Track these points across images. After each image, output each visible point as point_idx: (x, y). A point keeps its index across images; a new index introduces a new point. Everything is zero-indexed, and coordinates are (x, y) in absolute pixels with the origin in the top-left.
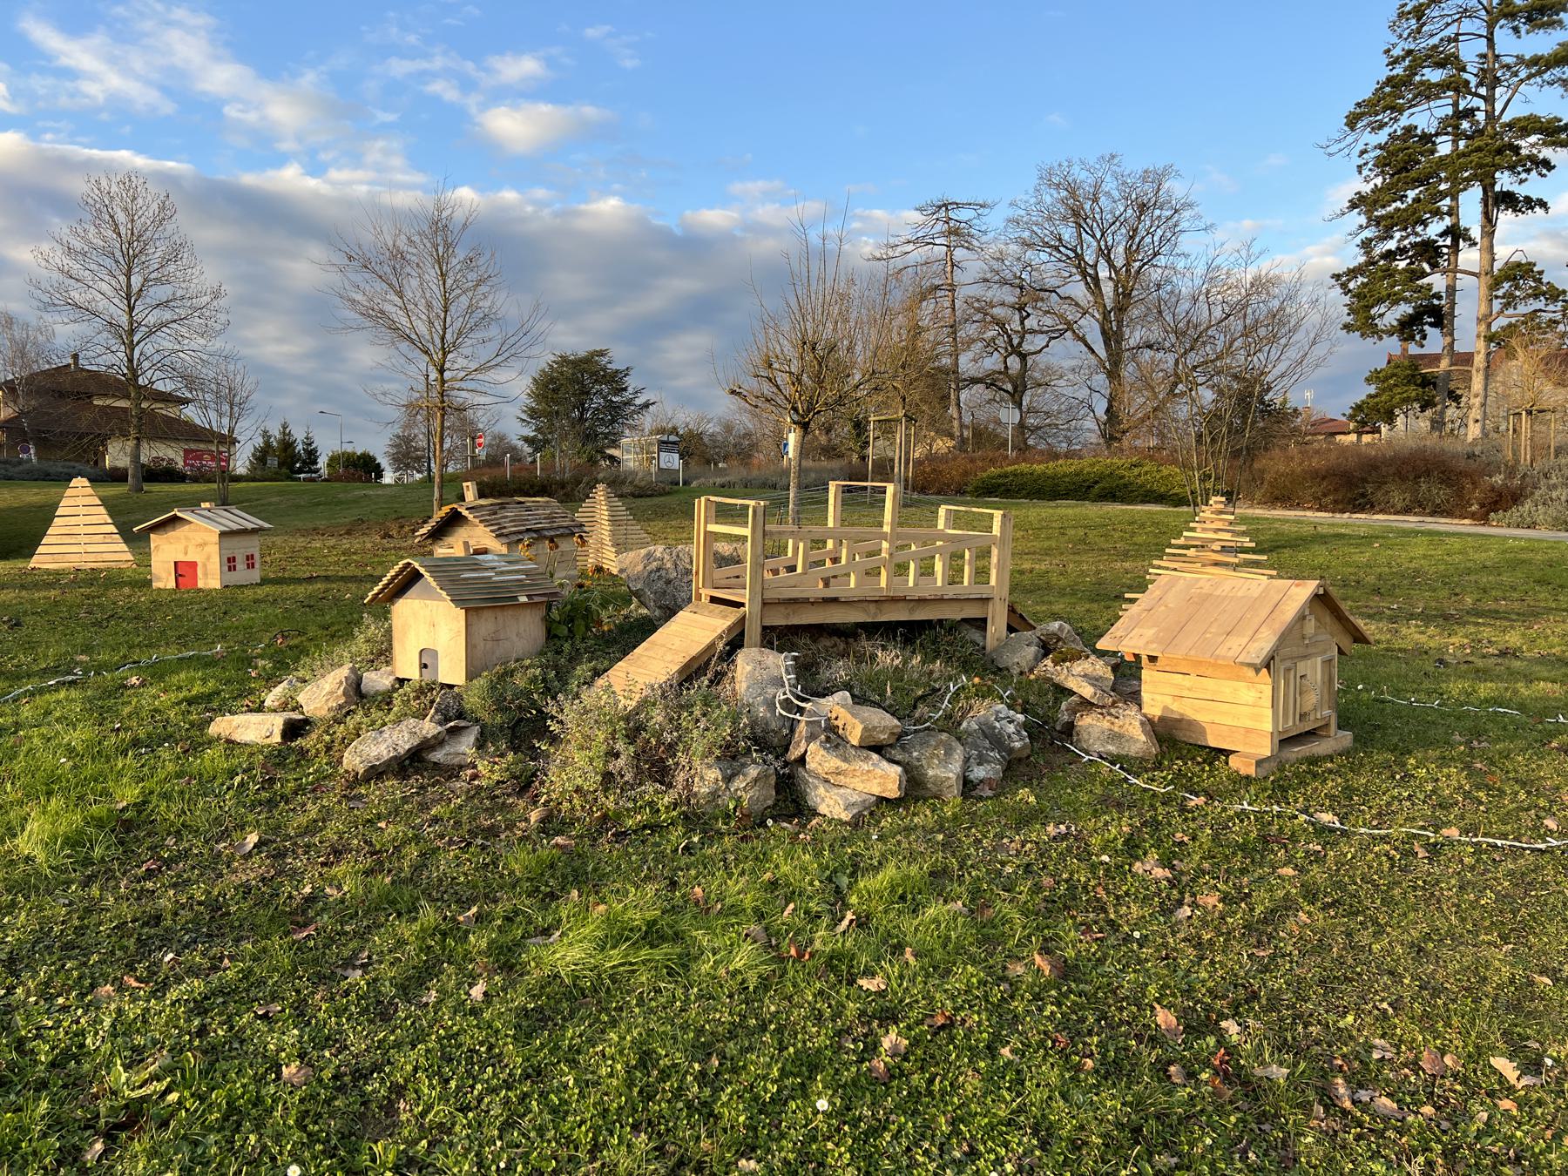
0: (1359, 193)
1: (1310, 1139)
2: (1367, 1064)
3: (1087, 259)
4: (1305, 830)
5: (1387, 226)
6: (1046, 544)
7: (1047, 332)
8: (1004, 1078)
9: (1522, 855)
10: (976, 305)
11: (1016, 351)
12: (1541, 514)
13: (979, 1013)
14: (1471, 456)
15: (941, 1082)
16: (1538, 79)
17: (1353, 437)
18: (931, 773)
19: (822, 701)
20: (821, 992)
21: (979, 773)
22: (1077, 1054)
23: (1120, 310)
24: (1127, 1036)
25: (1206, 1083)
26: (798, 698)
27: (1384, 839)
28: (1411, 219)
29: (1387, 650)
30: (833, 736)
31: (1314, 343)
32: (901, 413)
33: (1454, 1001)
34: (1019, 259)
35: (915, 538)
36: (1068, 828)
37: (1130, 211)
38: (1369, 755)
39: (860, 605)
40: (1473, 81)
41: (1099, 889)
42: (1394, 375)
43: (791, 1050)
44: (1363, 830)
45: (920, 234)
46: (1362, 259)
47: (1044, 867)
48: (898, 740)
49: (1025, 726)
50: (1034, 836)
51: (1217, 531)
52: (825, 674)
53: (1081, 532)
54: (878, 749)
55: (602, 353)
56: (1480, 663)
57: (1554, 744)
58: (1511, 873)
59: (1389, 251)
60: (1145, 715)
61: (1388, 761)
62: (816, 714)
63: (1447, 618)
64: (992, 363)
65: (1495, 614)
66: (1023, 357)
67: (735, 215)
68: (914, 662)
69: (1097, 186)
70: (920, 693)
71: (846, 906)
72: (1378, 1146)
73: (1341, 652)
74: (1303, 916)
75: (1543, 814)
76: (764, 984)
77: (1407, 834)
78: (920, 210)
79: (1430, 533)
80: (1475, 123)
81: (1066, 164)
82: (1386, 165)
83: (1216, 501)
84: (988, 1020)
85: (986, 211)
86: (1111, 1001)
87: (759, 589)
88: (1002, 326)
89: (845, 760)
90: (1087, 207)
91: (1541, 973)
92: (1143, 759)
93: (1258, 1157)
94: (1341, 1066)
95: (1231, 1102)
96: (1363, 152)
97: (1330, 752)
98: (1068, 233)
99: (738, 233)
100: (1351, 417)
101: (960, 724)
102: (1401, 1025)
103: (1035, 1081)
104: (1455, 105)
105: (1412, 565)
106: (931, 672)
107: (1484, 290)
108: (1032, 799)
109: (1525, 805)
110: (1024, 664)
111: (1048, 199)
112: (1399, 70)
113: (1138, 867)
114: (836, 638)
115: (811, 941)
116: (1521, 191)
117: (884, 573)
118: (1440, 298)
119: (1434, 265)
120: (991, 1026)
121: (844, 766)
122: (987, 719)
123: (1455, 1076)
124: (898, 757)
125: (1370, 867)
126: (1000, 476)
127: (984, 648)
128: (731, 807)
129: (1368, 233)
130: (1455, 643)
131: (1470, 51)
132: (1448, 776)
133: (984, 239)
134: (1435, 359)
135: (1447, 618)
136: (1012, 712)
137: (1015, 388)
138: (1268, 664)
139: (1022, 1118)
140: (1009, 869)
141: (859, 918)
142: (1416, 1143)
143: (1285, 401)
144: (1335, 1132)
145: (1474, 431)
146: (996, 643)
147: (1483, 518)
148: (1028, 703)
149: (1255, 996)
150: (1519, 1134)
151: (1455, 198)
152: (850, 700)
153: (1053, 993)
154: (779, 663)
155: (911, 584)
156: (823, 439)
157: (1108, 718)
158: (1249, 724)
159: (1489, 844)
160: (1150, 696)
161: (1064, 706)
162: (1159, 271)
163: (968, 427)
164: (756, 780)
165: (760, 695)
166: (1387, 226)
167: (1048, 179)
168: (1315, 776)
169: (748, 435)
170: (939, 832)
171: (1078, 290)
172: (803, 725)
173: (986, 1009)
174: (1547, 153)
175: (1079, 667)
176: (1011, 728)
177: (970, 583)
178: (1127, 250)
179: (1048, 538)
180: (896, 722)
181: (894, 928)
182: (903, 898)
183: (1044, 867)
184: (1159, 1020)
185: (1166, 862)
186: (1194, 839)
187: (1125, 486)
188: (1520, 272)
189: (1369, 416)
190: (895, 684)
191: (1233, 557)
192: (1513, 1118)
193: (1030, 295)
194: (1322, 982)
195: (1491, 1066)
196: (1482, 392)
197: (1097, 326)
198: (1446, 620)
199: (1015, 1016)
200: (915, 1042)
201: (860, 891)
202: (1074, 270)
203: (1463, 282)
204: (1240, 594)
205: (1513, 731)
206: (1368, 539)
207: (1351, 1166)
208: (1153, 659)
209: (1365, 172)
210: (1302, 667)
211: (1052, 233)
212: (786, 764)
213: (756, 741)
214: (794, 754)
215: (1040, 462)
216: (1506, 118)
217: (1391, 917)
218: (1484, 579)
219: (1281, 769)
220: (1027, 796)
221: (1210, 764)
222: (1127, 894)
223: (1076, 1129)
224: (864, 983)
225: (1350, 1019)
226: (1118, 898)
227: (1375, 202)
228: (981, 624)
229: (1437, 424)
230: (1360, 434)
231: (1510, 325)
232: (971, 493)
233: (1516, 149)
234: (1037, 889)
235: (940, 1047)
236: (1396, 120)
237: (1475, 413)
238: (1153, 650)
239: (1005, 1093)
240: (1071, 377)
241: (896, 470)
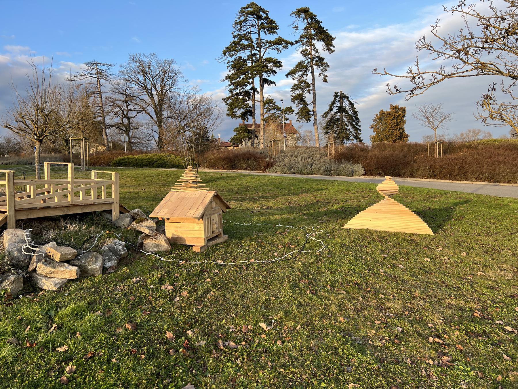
0: (228, 75)
1: (211, 361)
2: (228, 334)
3: (148, 87)
4: (214, 266)
5: (236, 85)
6: (139, 182)
7: (136, 111)
8: (112, 370)
9: (269, 264)
10: (110, 100)
11: (126, 116)
12: (278, 169)
13: (104, 349)
14: (261, 153)
15: (89, 377)
16: (271, 48)
17: (232, 148)
18: (89, 267)
19: (43, 246)
20: (40, 357)
21: (109, 264)
22: (140, 354)
23: (160, 105)
24: (157, 344)
25: (181, 352)
26: (33, 247)
27: (235, 265)
28: (242, 84)
29: (239, 210)
30: (48, 260)
31: (217, 119)
32: (82, 137)
33: (251, 309)
34: (124, 85)
35: (82, 183)
36: (140, 278)
37: (161, 73)
38: (232, 241)
39: (60, 209)
40: (255, 46)
41: (150, 297)
42: (241, 129)
43: (27, 382)
44: (229, 264)
45: (86, 73)
46: (230, 95)
47: (131, 293)
48: (76, 257)
49: (126, 246)
50: (128, 283)
51: (190, 177)
52: (45, 236)
53: (151, 178)
54: (68, 262)
55: (227, 115)
56: (262, 211)
57: (278, 232)
58: (266, 270)
59: (237, 93)
60: (167, 237)
61: (237, 242)
62: (40, 252)
63: (255, 199)
64: (118, 120)
65: (266, 197)
66: (129, 119)
67: (8, 58)
68: (83, 228)
69: (150, 63)
70: (85, 239)
71: (53, 322)
72: (230, 358)
73: (223, 212)
74: (212, 293)
75: (274, 252)
76: (16, 359)
77: (241, 263)
78: (86, 64)
79: (251, 175)
80: (256, 58)
81: (139, 55)
82: (235, 67)
83: (190, 167)
84: (108, 351)
85: (111, 67)
86: (152, 334)
87: (13, 205)
88: (120, 108)
89: (54, 268)
90: (147, 69)
91: (273, 297)
92: (166, 252)
93: (196, 371)
94: (221, 336)
95: (188, 356)
96: (228, 63)
97: (222, 241)
98: (141, 78)
99: (10, 66)
100: (231, 142)
101: (101, 248)
102: (237, 320)
103: (124, 368)
104: (251, 52)
105: (247, 185)
106: (90, 231)
107: (262, 106)
108: (128, 271)
109: (270, 250)
110: (126, 225)
111: (133, 66)
112: (236, 40)
113: (163, 287)
114: (50, 222)
115: (37, 339)
116: (269, 79)
117: (69, 196)
118: (251, 108)
119: (249, 98)
120: (109, 353)
121: (53, 270)
122: (111, 245)
123: (251, 331)
124: (76, 264)
125: (231, 274)
126: (122, 159)
127: (112, 220)
128: (2, 293)
129: (232, 87)
130: (256, 206)
131: (254, 37)
132: (252, 245)
133: (111, 77)
134: (251, 125)
135: (255, 199)
136: (121, 242)
137: (127, 129)
138: (202, 217)
139: (119, 382)
140: (118, 296)
141: (58, 325)
142: (240, 354)
143: (213, 137)
144: (218, 357)
145: (262, 146)
146: (116, 218)
147: (265, 171)
148: (127, 238)
149: (197, 321)
150: (266, 344)
151: (253, 79)
152: (56, 245)
153: (132, 335)
154: (23, 234)
155: (81, 199)
156: (52, 146)
157: (154, 240)
158: (198, 236)
159: (261, 262)
160: (168, 231)
161: (139, 237)
162: (172, 93)
163: (110, 142)
164: (13, 281)
165: (15, 247)
166: (236, 85)
167: (133, 59)
168: (217, 249)
169: (18, 144)
170: (93, 288)
171: (146, 97)
172: (35, 256)
173: (107, 347)
174: (274, 69)
175: (145, 224)
176: (121, 247)
177: (104, 198)
178: (161, 86)
179: (139, 181)
180: (75, 251)
181: (73, 326)
182: (77, 314)
183: (131, 293)
184: (167, 336)
185: (172, 284)
186: (181, 275)
187: (165, 162)
188: (270, 102)
189: (236, 141)
190: (75, 237)
191: (196, 184)
192: (265, 339)
193: (129, 98)
194: (216, 312)
195: (260, 326)
196: (263, 135)
197: (153, 110)
198: (254, 200)
199: (118, 347)
200: (79, 366)
201: (59, 316)
202: (144, 91)
203: (257, 104)
204: (193, 196)
205: (268, 229)
206: (235, 178)
207: (222, 366)
208: (168, 219)
209: (229, 69)
210: (212, 217)
211: (135, 77)
212: (28, 273)
213: (13, 265)
214: (31, 268)
215: (136, 155)
216: (264, 58)
217: (236, 288)
218: (265, 188)
219: (208, 249)
220: (126, 270)
221: (187, 250)
222: (159, 297)
223: (137, 380)
224: (59, 349)
225: (224, 321)
226: (156, 299)
227: (233, 78)
228: (110, 212)
229: (253, 144)
230: (234, 147)
231: (269, 117)
232: (113, 166)
233: (267, 67)
234: (129, 301)
235: (89, 365)
236: (236, 54)
237: (262, 141)
238: (167, 216)
239: (113, 375)
240: (146, 126)
241: (82, 157)
